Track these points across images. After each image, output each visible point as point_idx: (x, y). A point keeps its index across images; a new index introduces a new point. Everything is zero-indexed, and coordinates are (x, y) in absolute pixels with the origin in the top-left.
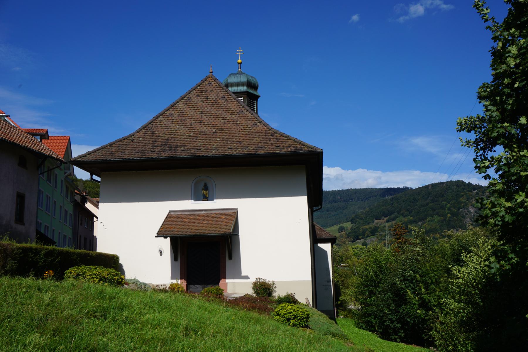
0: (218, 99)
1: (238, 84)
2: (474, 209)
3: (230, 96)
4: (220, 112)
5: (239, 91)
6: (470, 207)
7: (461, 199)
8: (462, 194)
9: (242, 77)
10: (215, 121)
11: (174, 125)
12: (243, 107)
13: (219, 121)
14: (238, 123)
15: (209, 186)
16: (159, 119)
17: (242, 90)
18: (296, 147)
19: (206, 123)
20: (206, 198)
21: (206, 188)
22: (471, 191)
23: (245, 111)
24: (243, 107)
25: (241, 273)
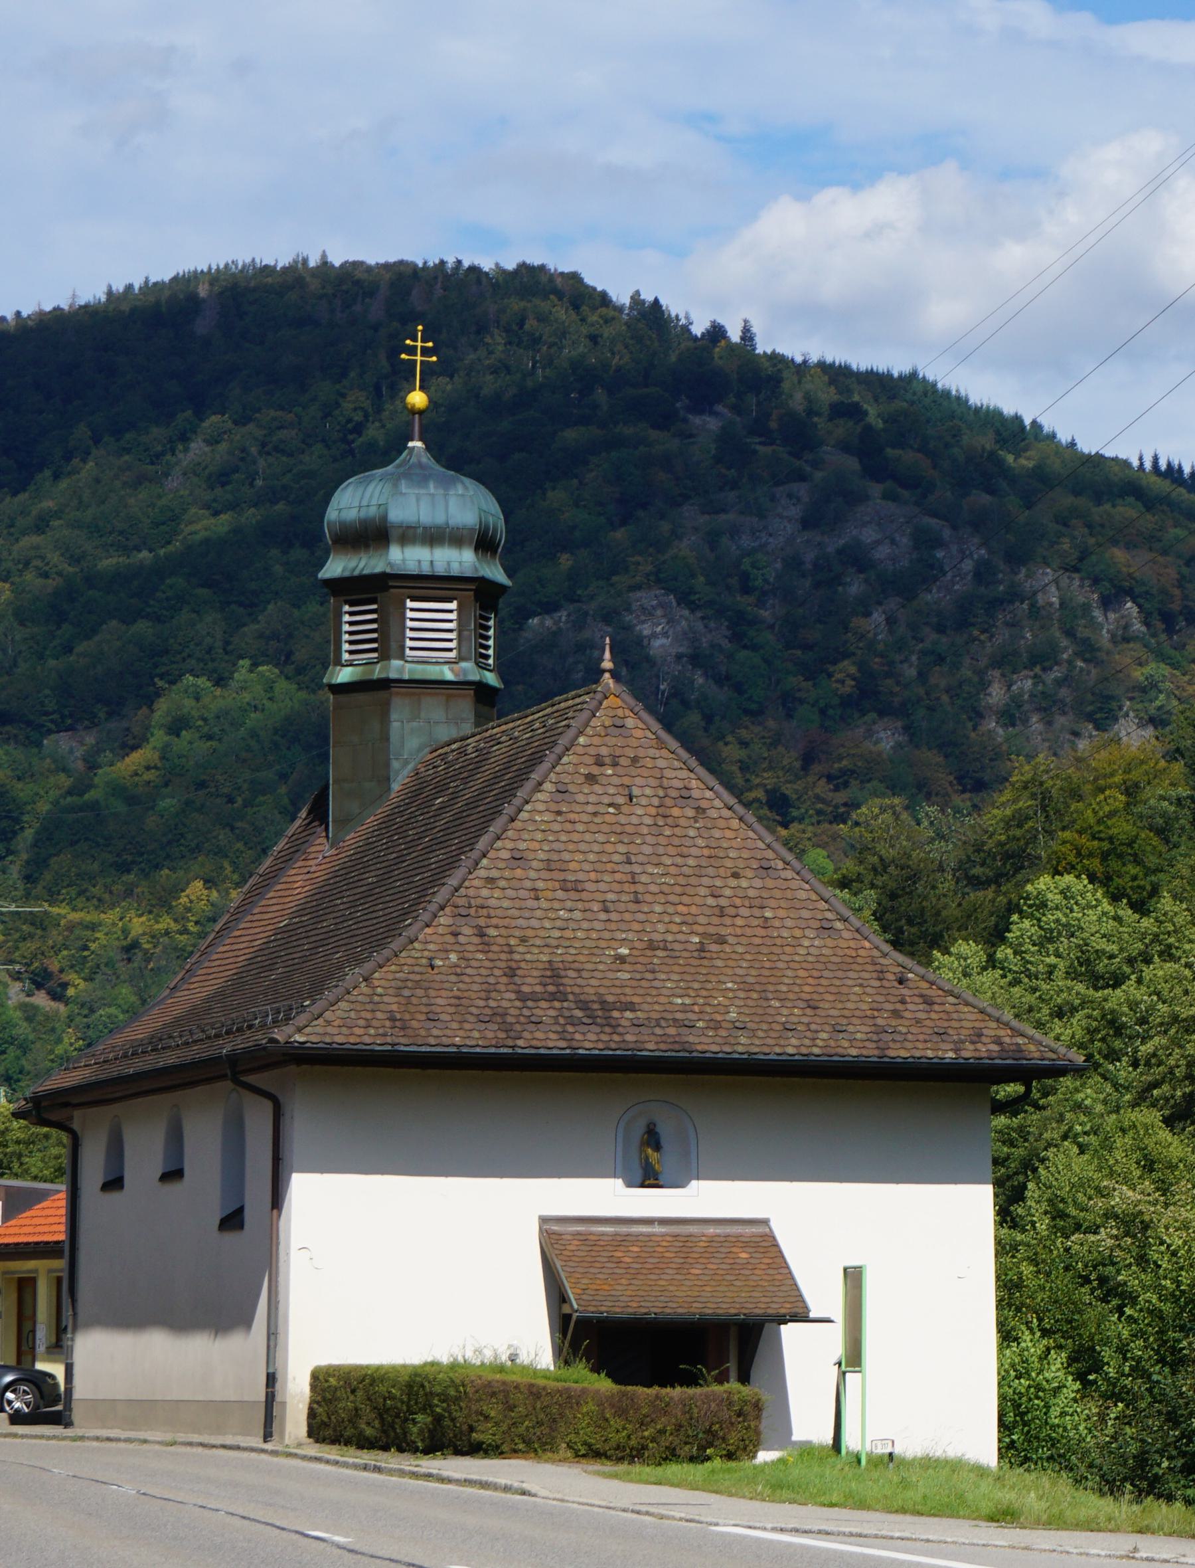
0: (669, 802)
1: (434, 536)
2: (685, 618)
3: (709, 794)
4: (691, 862)
5: (440, 570)
6: (647, 598)
7: (556, 496)
8: (571, 435)
9: (453, 502)
10: (685, 899)
11: (544, 904)
12: (769, 846)
13: (697, 900)
14: (768, 914)
15: (665, 1131)
16: (482, 873)
17: (455, 570)
18: (998, 1041)
19: (658, 909)
20: (649, 1178)
21: (652, 1139)
22: (665, 420)
23: (780, 865)
24: (769, 846)
25: (790, 1433)
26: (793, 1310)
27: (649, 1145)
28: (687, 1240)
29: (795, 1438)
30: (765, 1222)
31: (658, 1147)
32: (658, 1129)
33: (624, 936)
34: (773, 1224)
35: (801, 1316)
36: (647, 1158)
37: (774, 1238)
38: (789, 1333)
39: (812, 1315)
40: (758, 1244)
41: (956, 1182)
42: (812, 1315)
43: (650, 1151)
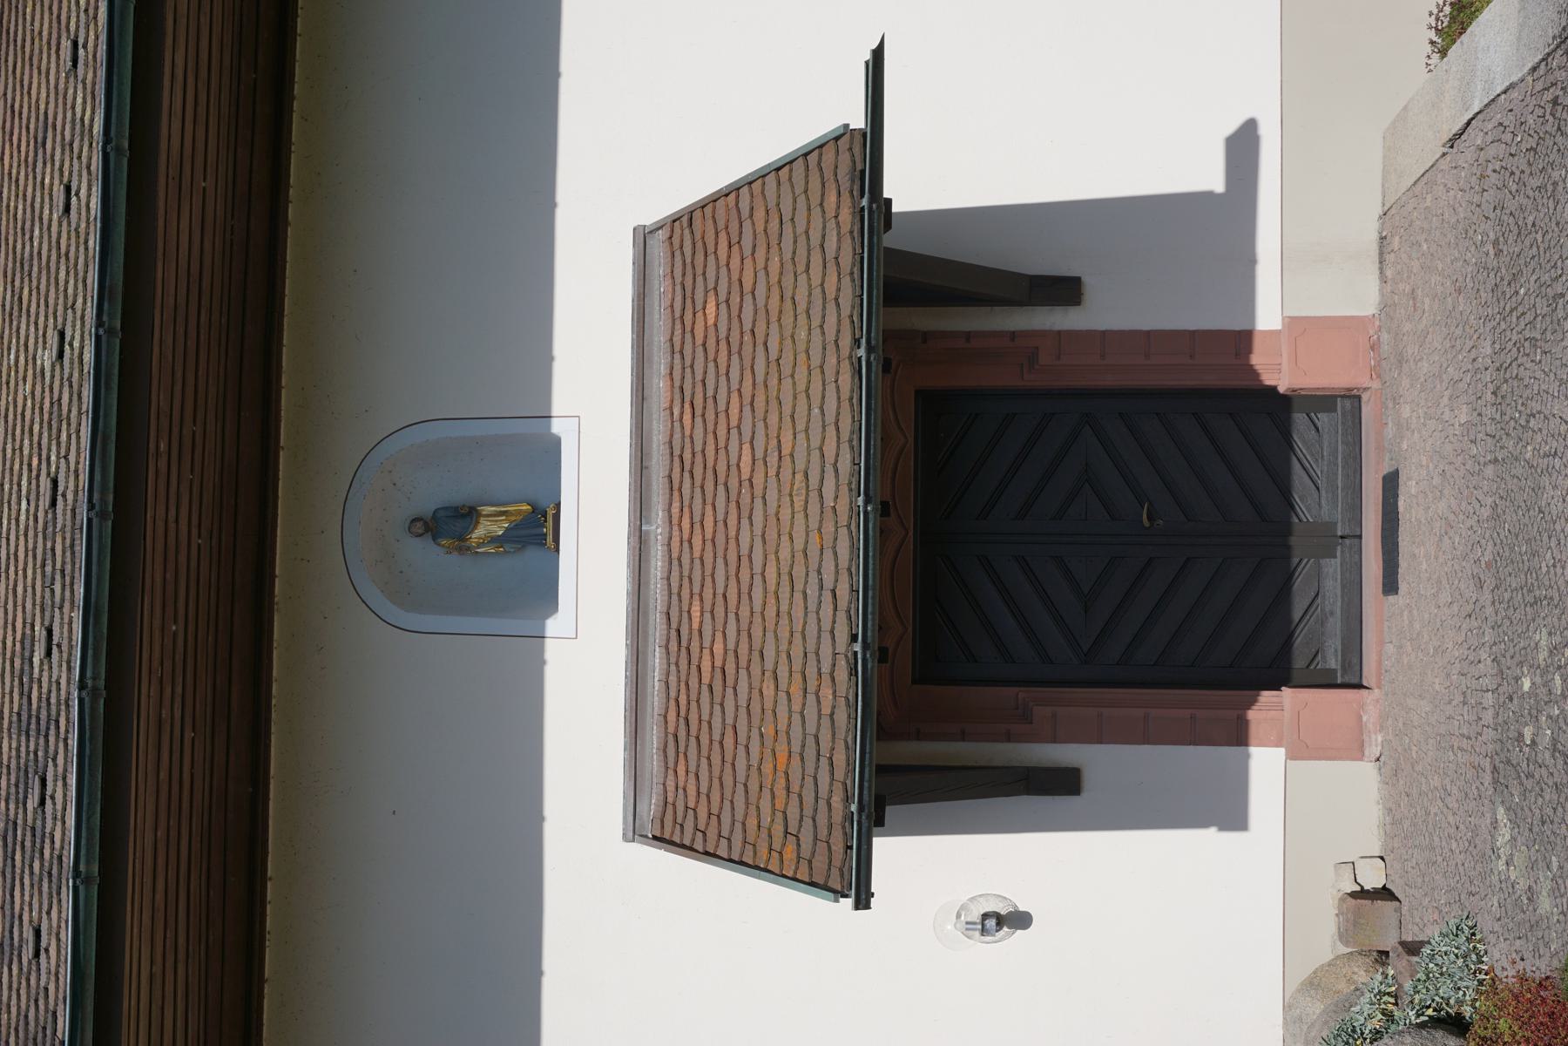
15: (431, 493)
20: (537, 529)
21: (449, 524)
25: (1208, 196)
26: (845, 184)
27: (462, 537)
28: (681, 468)
29: (1218, 184)
30: (643, 237)
31: (467, 514)
32: (427, 507)
33: (817, 410)
34: (650, 218)
35: (862, 150)
36: (494, 540)
37: (675, 219)
38: (910, 187)
39: (858, 121)
40: (693, 251)
41: (536, 973)
42: (858, 121)
43: (479, 532)
